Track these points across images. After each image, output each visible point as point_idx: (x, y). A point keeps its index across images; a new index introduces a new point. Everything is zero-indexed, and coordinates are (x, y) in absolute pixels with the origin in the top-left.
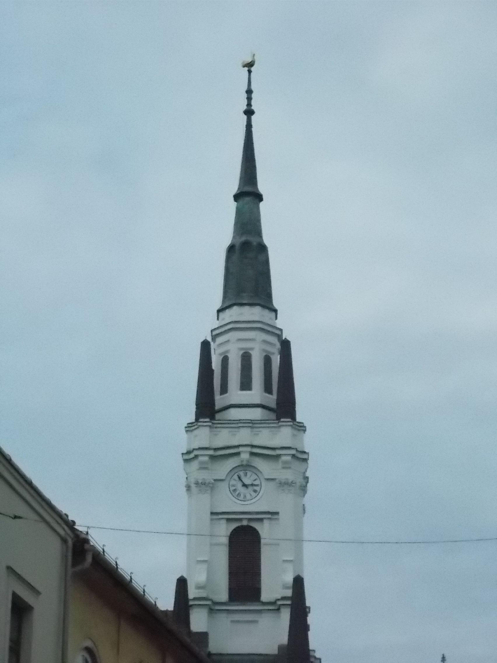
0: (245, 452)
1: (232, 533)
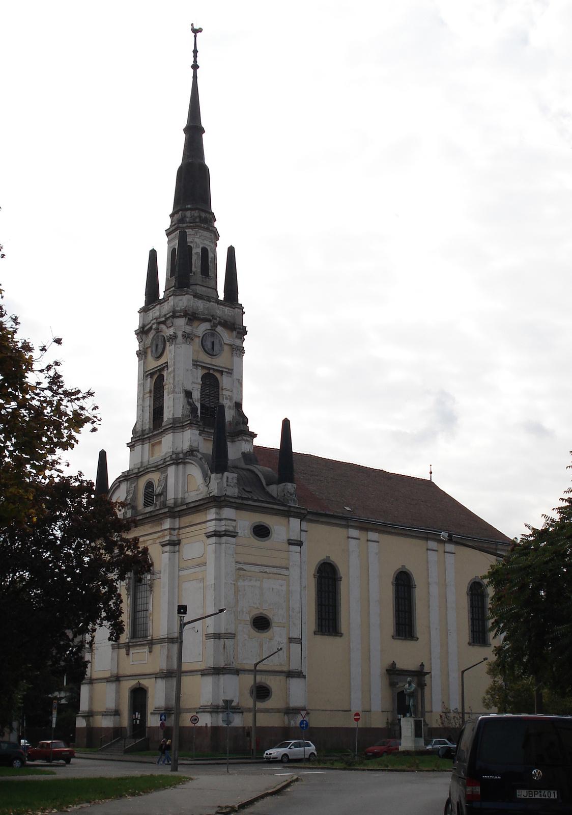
0: (168, 461)
1: (140, 362)
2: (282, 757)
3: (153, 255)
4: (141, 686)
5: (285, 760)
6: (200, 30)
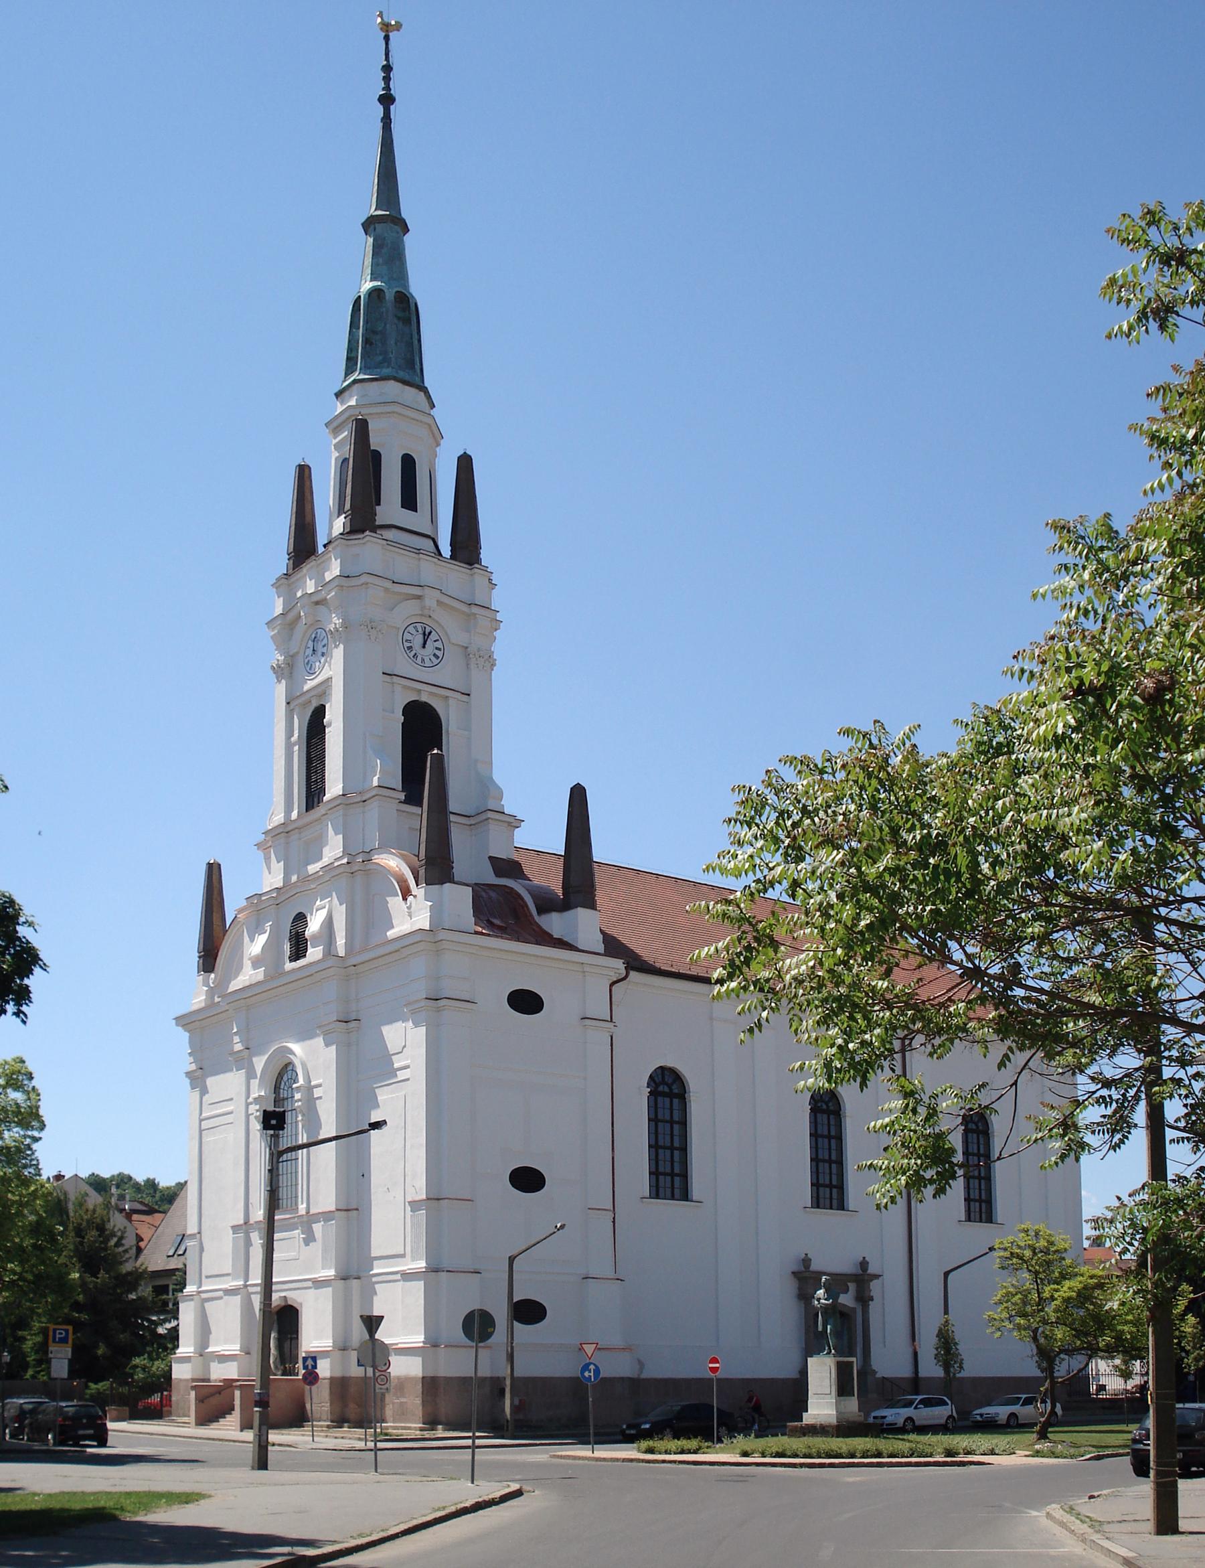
2: (904, 1423)
3: (303, 474)
4: (290, 1303)
5: (909, 1426)
6: (398, 26)
